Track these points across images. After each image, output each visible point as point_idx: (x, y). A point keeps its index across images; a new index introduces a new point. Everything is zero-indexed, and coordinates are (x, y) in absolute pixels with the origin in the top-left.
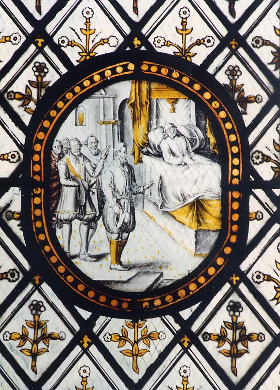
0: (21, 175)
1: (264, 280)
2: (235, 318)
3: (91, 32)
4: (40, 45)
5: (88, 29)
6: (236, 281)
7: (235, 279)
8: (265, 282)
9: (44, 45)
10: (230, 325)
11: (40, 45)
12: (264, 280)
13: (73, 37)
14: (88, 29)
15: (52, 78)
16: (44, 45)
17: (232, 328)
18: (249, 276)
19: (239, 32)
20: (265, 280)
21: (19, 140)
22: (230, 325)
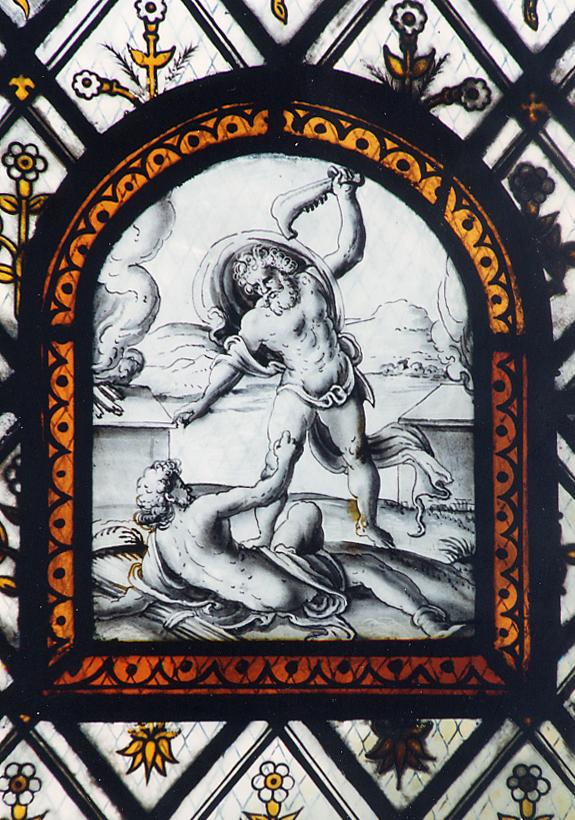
0: (51, 663)
1: (100, 91)
2: (24, 185)
3: (161, 59)
4: (21, 94)
5: (152, 50)
6: (27, 88)
7: (22, 85)
8: (105, 97)
9: (33, 94)
10: (13, 200)
11: (21, 94)
12: (100, 91)
13: (113, 71)
14: (152, 50)
15: (52, 179)
16: (33, 94)
17: (17, 210)
18: (64, 79)
19: (485, 159)
20: (104, 92)
21: (254, 746)
22: (13, 200)
